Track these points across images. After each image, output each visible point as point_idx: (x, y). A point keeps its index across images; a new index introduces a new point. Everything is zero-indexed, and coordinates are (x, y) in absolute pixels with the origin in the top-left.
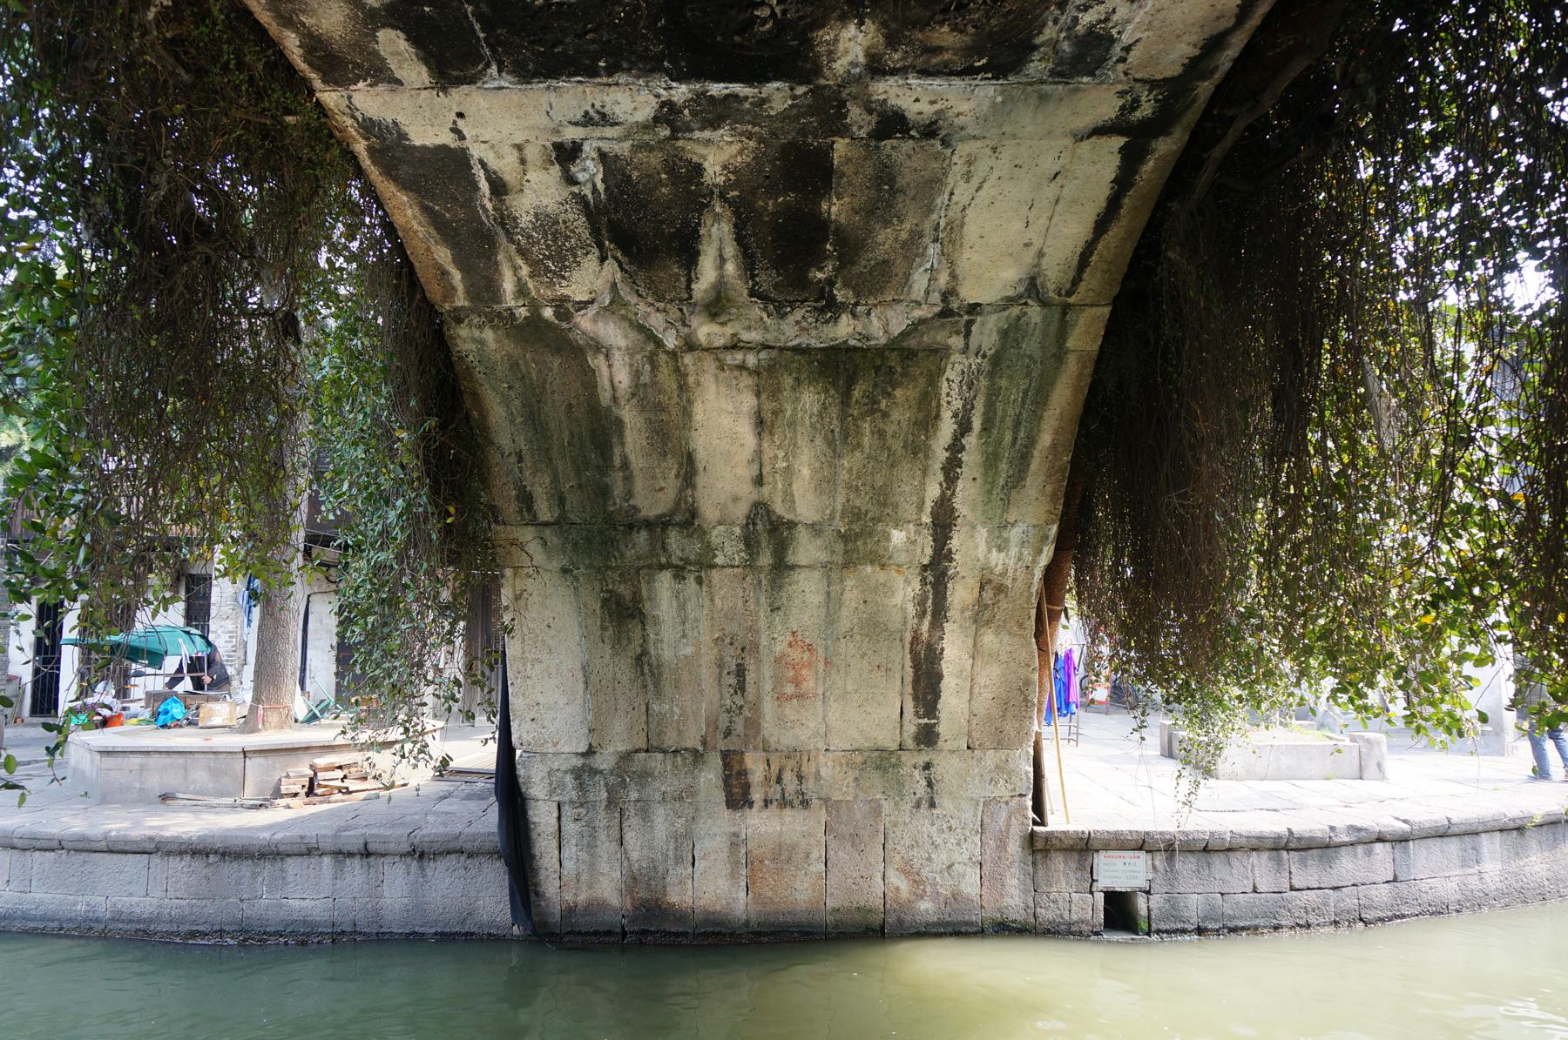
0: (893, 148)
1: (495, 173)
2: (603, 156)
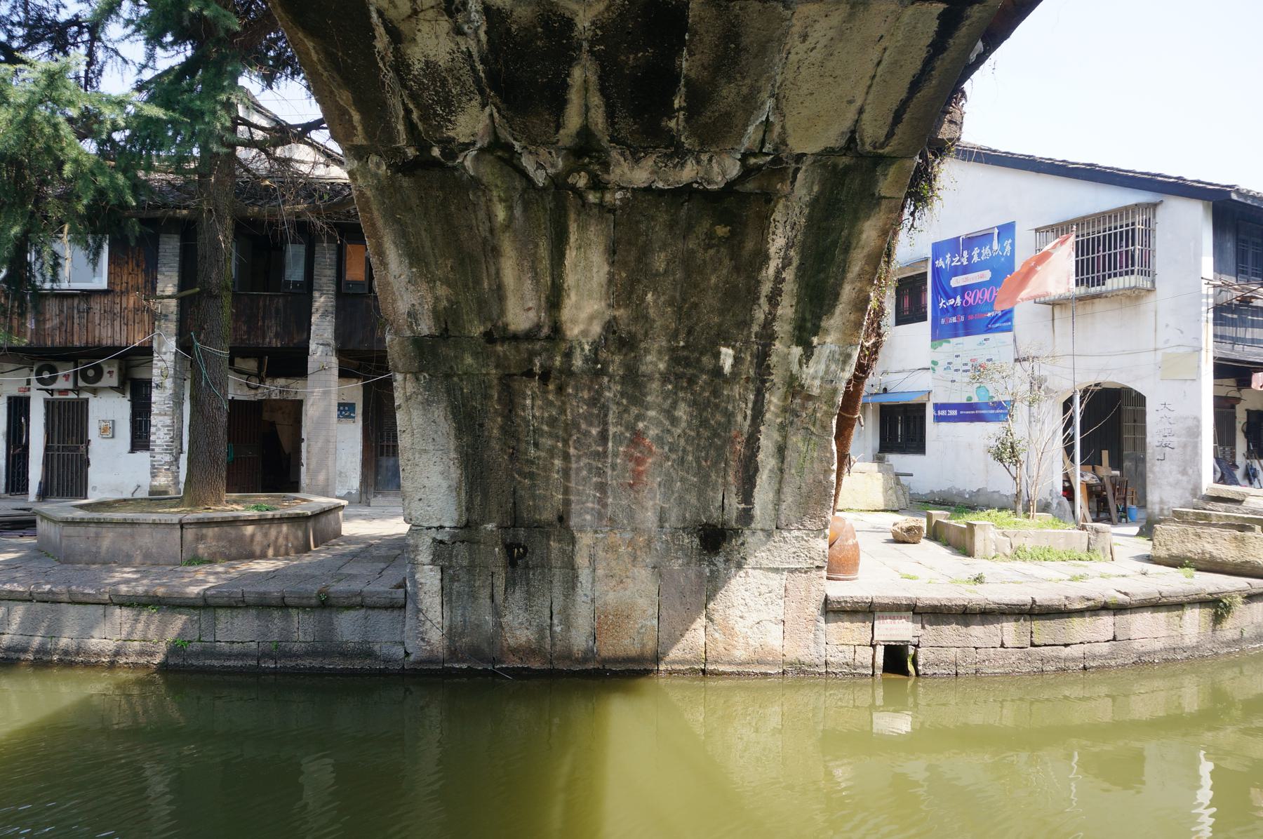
0: (741, 9)
1: (391, 22)
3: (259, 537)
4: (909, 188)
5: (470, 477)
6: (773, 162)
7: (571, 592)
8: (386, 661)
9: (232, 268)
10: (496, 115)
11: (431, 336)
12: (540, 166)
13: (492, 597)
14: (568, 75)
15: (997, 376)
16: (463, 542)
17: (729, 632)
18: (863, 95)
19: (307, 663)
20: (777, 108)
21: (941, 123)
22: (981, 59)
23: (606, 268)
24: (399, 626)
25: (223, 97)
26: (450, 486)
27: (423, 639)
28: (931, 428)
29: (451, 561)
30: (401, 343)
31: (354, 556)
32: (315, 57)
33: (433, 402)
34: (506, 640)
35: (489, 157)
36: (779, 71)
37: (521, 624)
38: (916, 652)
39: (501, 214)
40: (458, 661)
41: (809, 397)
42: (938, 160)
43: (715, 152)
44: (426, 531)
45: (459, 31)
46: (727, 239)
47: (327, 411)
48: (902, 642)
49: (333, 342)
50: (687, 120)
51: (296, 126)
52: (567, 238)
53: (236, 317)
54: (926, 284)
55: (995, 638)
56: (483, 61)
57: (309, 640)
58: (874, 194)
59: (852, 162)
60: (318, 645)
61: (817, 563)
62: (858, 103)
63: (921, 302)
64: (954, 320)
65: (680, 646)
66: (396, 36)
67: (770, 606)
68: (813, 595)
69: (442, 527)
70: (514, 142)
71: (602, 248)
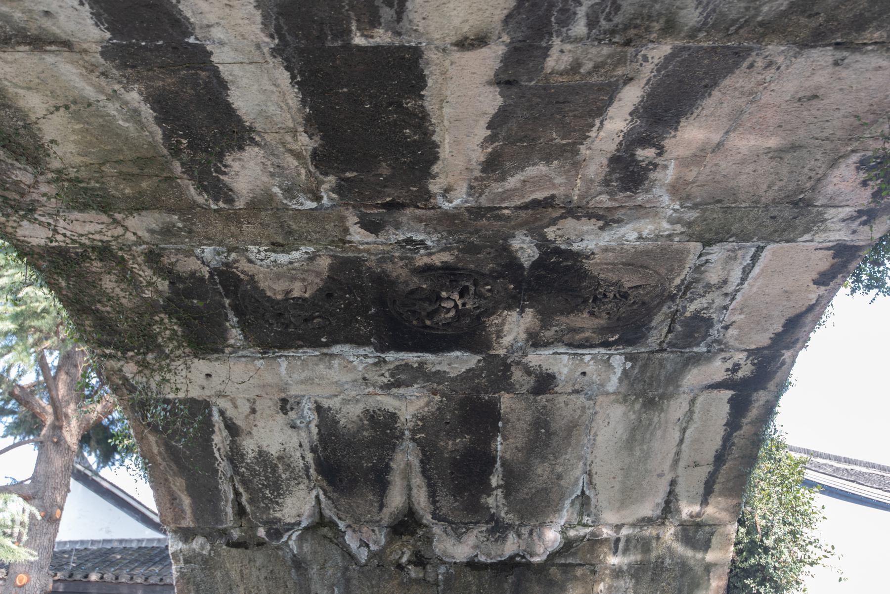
0: (547, 401)
1: (231, 419)
2: (319, 409)
10: (322, 497)
32: (155, 450)
50: (506, 496)
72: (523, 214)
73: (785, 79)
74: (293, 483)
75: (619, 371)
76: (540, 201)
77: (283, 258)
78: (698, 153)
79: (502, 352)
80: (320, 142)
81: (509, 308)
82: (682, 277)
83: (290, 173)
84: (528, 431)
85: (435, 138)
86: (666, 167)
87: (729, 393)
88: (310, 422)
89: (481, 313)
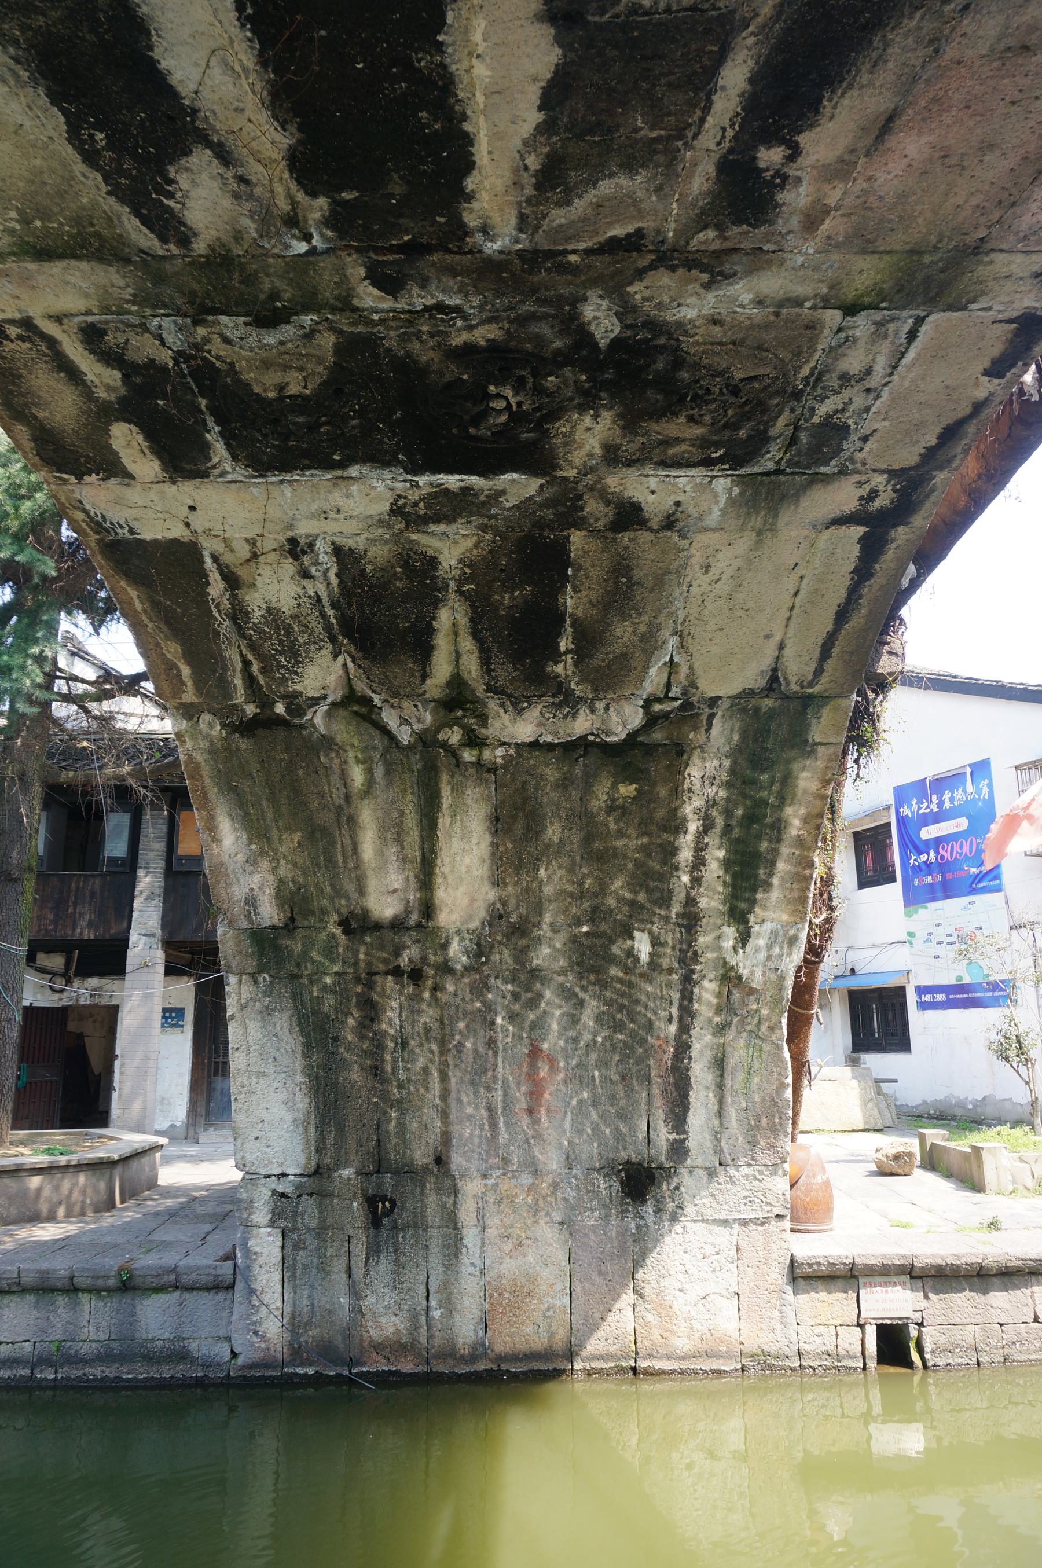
0: (630, 540)
1: (227, 567)
2: (338, 551)
3: (47, 1192)
4: (849, 731)
5: (321, 1107)
6: (682, 707)
7: (453, 1261)
8: (206, 1365)
9: (40, 844)
10: (350, 665)
11: (274, 927)
12: (405, 721)
13: (349, 1271)
14: (434, 618)
15: (989, 950)
16: (311, 1194)
17: (665, 1312)
18: (782, 628)
19: (97, 1371)
20: (682, 647)
21: (878, 654)
22: (915, 584)
23: (488, 838)
24: (225, 1314)
25: (35, 650)
26: (295, 1120)
27: (256, 1333)
28: (916, 1019)
29: (295, 1220)
30: (237, 937)
31: (172, 1214)
32: (139, 607)
33: (275, 1010)
34: (367, 1332)
35: (342, 713)
36: (681, 605)
37: (388, 1307)
38: (920, 1332)
39: (357, 776)
40: (302, 1365)
41: (752, 991)
42: (881, 697)
43: (613, 699)
44: (263, 1181)
45: (305, 574)
46: (634, 798)
47: (147, 1020)
48: (900, 1319)
49: (159, 932)
50: (576, 664)
51: (126, 677)
52: (439, 805)
53: (41, 903)
54: (890, 837)
55: (1025, 1309)
56: (334, 606)
57: (102, 1338)
58: (807, 741)
59: (777, 704)
60: (114, 1345)
61: (777, 1211)
62: (777, 638)
63: (886, 859)
64: (929, 879)
65: (600, 1334)
66: (232, 581)
67: (718, 1273)
68: (775, 1256)
69: (284, 1175)
70: (373, 695)
71: (482, 814)
72: (599, 262)
73: (984, 12)
74: (312, 648)
75: (723, 499)
76: (622, 239)
77: (270, 339)
78: (846, 157)
79: (571, 473)
80: (298, 135)
81: (582, 409)
82: (812, 364)
83: (694, 694)
84: (605, 580)
85: (467, 127)
86: (799, 180)
87: (859, 530)
88: (328, 569)
89: (542, 416)
